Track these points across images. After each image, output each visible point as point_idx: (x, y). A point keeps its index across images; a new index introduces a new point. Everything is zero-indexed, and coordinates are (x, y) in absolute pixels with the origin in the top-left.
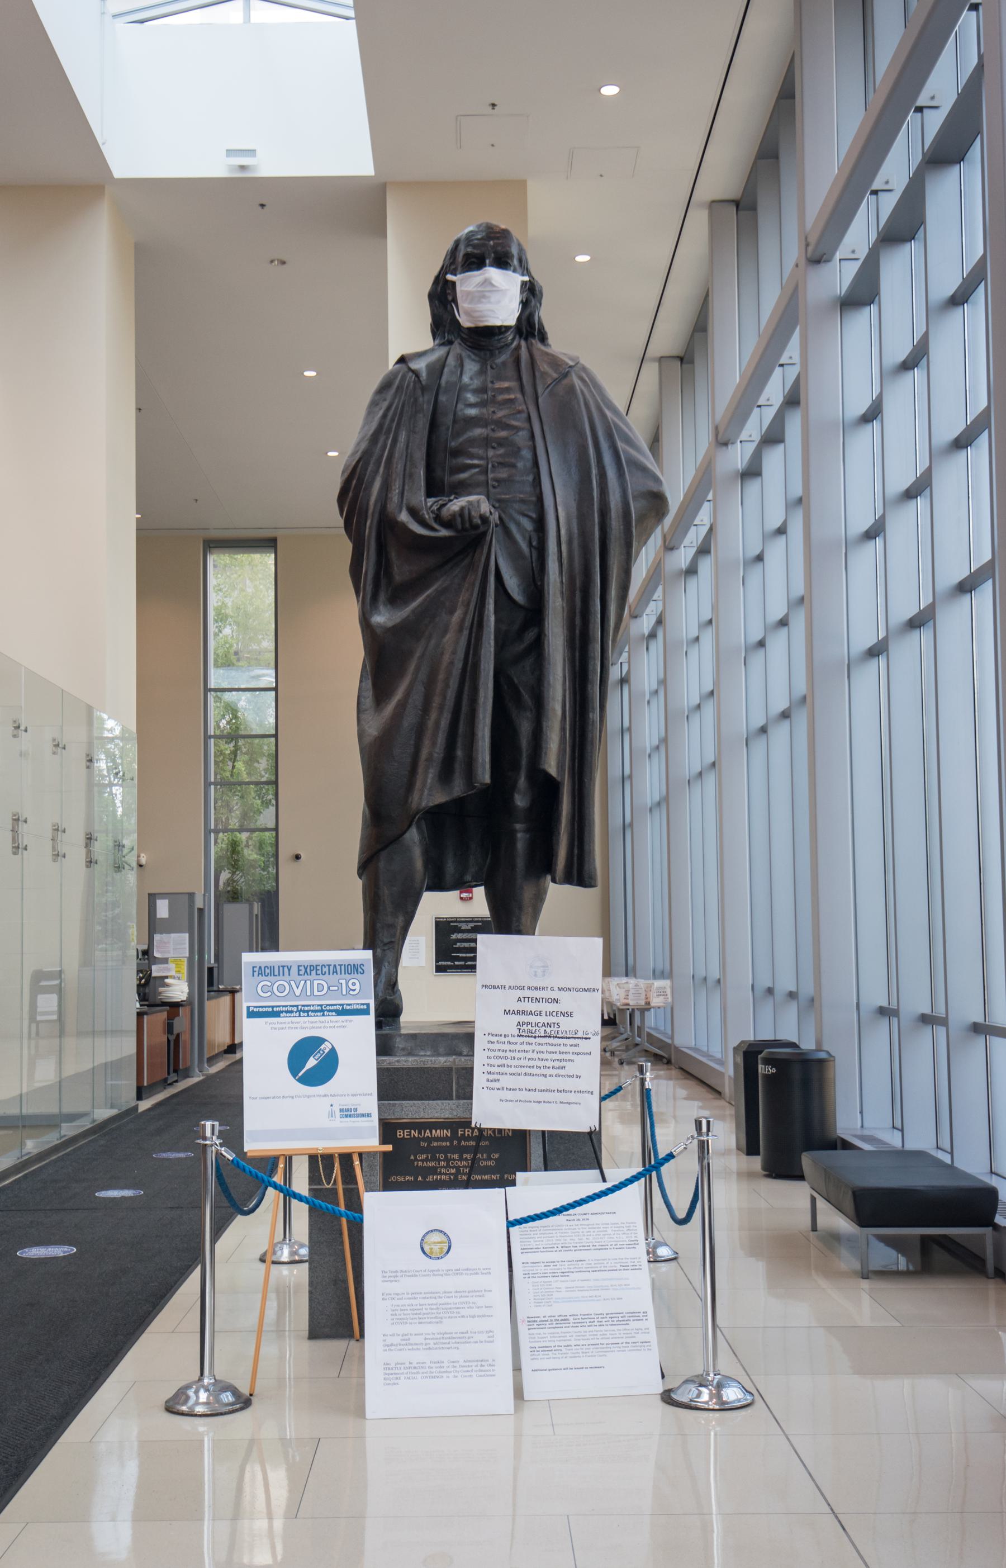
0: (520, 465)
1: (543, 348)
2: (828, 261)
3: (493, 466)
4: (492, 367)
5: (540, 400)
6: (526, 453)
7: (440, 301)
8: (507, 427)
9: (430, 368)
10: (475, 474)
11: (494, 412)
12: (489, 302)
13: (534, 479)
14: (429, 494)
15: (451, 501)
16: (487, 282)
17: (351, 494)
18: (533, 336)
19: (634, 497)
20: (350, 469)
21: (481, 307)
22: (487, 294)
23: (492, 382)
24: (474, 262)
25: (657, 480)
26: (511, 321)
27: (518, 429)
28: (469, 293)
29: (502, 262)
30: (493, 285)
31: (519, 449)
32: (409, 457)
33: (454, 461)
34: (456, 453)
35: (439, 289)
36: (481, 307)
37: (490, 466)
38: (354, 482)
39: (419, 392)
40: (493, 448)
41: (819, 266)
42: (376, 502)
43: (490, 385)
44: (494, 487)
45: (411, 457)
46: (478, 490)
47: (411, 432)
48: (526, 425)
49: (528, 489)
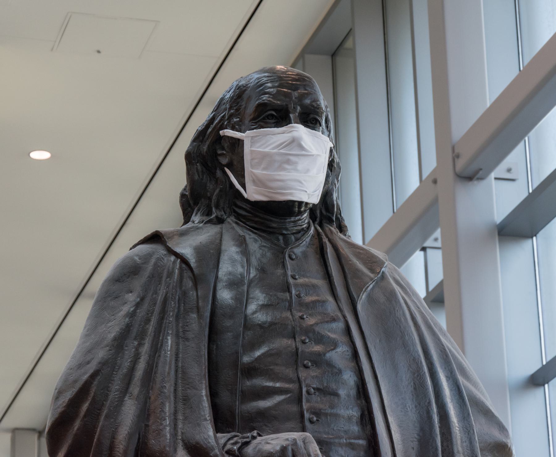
0: (342, 392)
1: (342, 236)
2: (482, 179)
3: (308, 393)
4: (290, 257)
5: (359, 307)
6: (349, 377)
7: (204, 164)
8: (320, 339)
9: (199, 251)
10: (280, 403)
11: (302, 318)
12: (296, 170)
13: (362, 416)
14: (218, 430)
15: (254, 438)
16: (295, 142)
17: (77, 424)
18: (330, 221)
19: (481, 450)
20: (79, 385)
21: (282, 175)
22: (292, 158)
23: (294, 277)
24: (274, 114)
25: (502, 428)
26: (314, 198)
27: (334, 345)
28: (265, 156)
29: (310, 119)
30: (301, 147)
31: (340, 372)
32: (181, 374)
33: (248, 383)
34: (250, 371)
35: (205, 148)
36: (282, 175)
37: (304, 390)
38: (85, 407)
39: (189, 284)
40: (306, 367)
41: (471, 183)
42: (130, 436)
43: (291, 280)
44: (311, 422)
45: (184, 373)
46: (289, 425)
47: (181, 337)
48: (344, 339)
49: (355, 428)
